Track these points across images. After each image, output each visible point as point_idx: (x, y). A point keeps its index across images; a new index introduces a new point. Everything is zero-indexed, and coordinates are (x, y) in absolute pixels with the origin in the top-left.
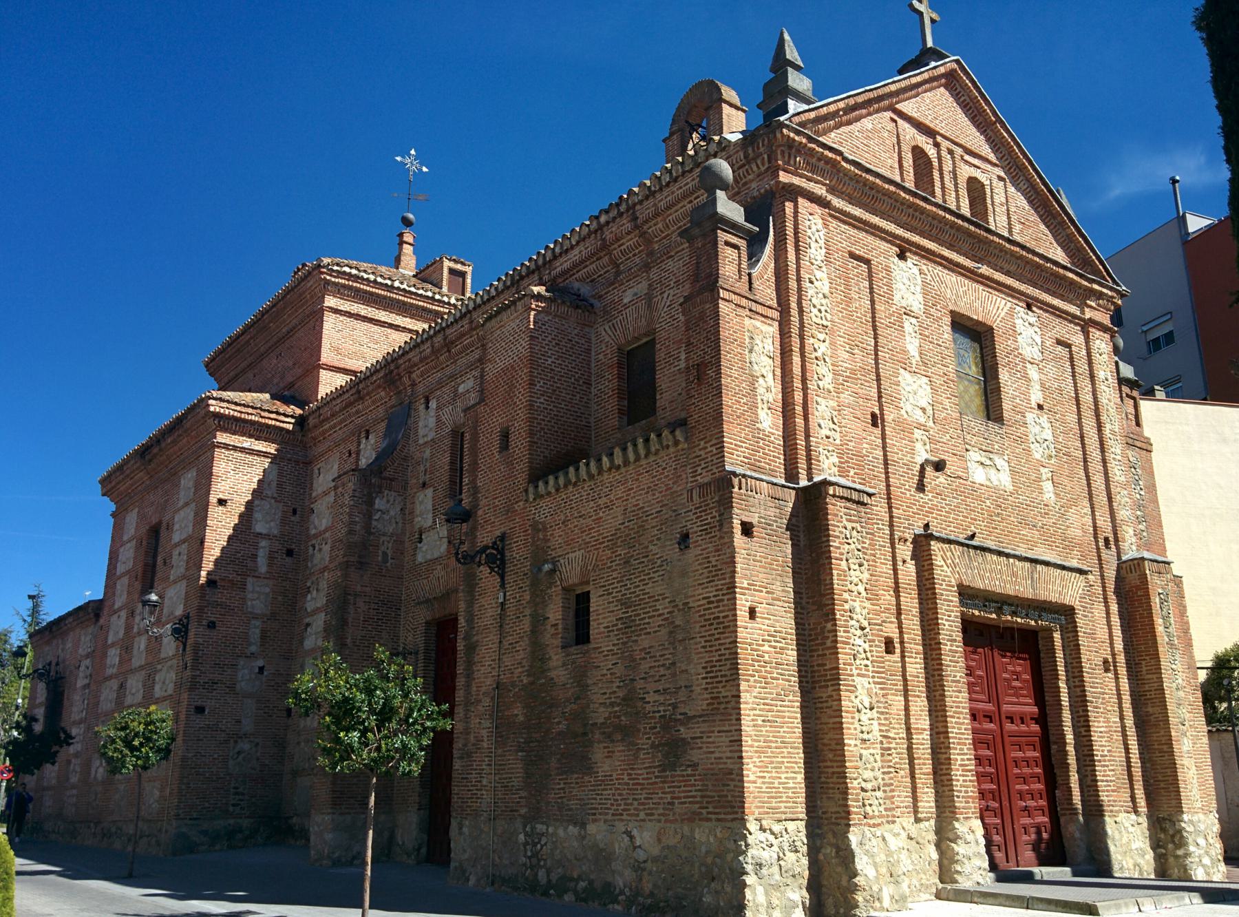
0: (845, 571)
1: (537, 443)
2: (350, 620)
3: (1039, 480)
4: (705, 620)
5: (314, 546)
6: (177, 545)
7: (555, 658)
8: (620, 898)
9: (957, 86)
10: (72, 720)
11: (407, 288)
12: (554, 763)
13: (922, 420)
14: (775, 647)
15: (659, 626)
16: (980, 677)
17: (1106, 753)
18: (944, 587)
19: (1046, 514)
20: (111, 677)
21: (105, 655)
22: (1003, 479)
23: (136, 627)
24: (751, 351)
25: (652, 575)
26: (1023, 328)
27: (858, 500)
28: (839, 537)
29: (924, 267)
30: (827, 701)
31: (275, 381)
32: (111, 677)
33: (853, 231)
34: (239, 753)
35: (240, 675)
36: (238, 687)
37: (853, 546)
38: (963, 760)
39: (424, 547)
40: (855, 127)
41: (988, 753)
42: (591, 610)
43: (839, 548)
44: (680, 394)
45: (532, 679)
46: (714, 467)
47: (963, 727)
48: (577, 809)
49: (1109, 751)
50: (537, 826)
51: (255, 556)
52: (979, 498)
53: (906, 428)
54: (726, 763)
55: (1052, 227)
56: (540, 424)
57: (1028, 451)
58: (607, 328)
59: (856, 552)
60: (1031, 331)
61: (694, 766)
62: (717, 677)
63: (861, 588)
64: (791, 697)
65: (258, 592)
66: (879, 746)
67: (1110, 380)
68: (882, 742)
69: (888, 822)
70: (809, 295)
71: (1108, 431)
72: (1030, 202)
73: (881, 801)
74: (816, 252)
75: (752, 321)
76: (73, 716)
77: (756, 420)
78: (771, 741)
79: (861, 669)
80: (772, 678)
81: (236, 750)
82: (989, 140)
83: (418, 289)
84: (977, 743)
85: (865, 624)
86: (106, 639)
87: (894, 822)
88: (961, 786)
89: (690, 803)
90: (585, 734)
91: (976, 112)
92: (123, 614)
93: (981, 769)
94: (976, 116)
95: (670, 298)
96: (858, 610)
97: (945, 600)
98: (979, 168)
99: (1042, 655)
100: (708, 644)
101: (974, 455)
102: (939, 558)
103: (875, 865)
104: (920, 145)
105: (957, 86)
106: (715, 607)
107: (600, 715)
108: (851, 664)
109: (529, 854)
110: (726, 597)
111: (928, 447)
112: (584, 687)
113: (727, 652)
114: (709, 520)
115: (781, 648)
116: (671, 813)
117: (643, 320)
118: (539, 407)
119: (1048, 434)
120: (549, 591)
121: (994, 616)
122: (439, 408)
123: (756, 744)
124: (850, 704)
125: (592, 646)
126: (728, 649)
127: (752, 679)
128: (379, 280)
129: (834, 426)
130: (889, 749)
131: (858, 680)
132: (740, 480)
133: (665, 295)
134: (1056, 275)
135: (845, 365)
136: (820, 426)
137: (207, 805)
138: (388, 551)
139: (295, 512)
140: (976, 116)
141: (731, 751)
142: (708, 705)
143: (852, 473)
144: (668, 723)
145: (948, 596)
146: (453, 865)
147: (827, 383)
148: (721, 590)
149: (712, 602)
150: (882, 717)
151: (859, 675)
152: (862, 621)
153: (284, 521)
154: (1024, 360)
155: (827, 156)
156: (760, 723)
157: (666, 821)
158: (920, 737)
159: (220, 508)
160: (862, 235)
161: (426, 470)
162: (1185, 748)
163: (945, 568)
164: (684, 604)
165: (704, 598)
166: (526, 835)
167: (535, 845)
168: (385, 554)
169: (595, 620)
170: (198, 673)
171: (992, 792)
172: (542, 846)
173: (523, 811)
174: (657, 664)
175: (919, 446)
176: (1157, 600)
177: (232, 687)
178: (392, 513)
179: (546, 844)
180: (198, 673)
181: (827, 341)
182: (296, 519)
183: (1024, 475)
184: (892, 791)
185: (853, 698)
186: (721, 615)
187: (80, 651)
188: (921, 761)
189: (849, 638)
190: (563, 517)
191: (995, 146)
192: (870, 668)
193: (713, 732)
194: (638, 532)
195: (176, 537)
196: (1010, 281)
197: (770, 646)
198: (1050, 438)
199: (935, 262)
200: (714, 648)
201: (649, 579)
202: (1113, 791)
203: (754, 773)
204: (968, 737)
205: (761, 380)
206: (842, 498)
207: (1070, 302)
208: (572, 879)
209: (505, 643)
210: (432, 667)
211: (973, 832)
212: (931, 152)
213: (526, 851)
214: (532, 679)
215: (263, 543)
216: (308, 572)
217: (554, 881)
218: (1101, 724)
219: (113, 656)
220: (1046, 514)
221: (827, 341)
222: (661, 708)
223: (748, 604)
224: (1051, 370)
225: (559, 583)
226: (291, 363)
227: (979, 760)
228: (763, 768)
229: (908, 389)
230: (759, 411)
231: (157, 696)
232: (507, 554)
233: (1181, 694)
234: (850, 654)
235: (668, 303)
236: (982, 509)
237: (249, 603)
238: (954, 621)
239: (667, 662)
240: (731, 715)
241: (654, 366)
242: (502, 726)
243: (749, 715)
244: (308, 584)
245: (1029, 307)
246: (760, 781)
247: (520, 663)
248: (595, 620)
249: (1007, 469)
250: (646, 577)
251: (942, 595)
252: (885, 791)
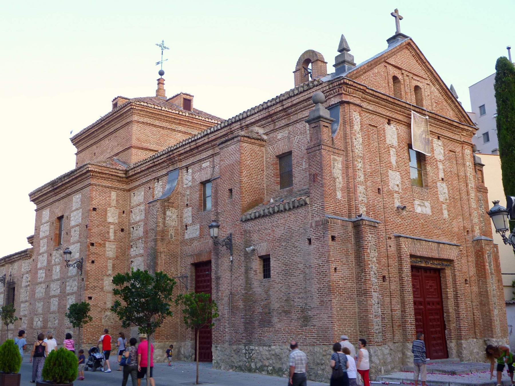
0: (369, 253)
1: (244, 197)
2: (159, 263)
3: (442, 210)
4: (318, 272)
5: (133, 228)
6: (73, 227)
7: (255, 284)
8: (285, 373)
10: (21, 300)
11: (168, 110)
12: (257, 323)
13: (397, 190)
14: (344, 282)
15: (299, 274)
16: (418, 289)
17: (465, 316)
18: (405, 256)
19: (444, 223)
20: (40, 283)
21: (37, 273)
22: (428, 211)
23: (53, 261)
24: (334, 168)
25: (296, 254)
26: (436, 147)
27: (374, 226)
28: (367, 240)
29: (398, 127)
30: (362, 302)
31: (108, 151)
32: (40, 283)
33: (371, 116)
34: (106, 316)
35: (105, 283)
36: (104, 288)
37: (372, 243)
38: (411, 321)
39: (188, 231)
41: (420, 317)
42: (271, 266)
43: (367, 245)
44: (303, 179)
45: (246, 291)
46: (321, 215)
47: (411, 308)
48: (267, 341)
49: (466, 315)
50: (250, 347)
51: (108, 232)
52: (418, 219)
53: (391, 193)
54: (326, 325)
56: (245, 189)
57: (438, 198)
58: (270, 148)
59: (373, 246)
60: (440, 148)
61: (314, 326)
62: (323, 293)
63: (374, 259)
64: (349, 300)
65: (110, 248)
66: (381, 317)
67: (471, 166)
68: (382, 316)
69: (384, 344)
70: (355, 144)
71: (470, 187)
74: (357, 127)
75: (334, 156)
76: (21, 298)
77: (336, 196)
78: (342, 316)
79: (374, 289)
80: (343, 293)
81: (105, 315)
83: (172, 110)
84: (416, 314)
85: (376, 272)
86: (37, 265)
87: (386, 344)
88: (410, 330)
89: (313, 338)
90: (269, 313)
92: (46, 255)
93: (417, 323)
95: (298, 139)
96: (374, 267)
97: (405, 261)
98: (419, 81)
99: (441, 279)
100: (319, 281)
101: (417, 202)
102: (403, 245)
103: (379, 359)
104: (396, 75)
106: (322, 268)
107: (275, 305)
108: (371, 288)
109: (247, 357)
110: (326, 264)
111: (399, 200)
112: (269, 296)
113: (327, 284)
114: (319, 235)
115: (346, 282)
116: (305, 342)
117: (286, 146)
118: (245, 182)
119: (446, 190)
120: (252, 257)
122: (193, 173)
123: (337, 317)
125: (272, 279)
126: (327, 283)
127: (336, 294)
128: (156, 107)
129: (364, 196)
130: (384, 318)
131: (373, 293)
132: (331, 220)
133: (296, 138)
135: (368, 171)
137: (94, 338)
138: (173, 234)
139: (124, 212)
141: (328, 320)
142: (319, 303)
143: (371, 214)
144: (303, 310)
145: (406, 259)
146: (213, 361)
147: (362, 178)
148: (324, 261)
149: (321, 266)
150: (382, 306)
151: (374, 291)
152: (375, 271)
153: (119, 217)
154: (437, 161)
156: (339, 310)
157: (303, 345)
158: (395, 312)
159: (94, 212)
160: (374, 116)
161: (188, 199)
162: (495, 313)
163: (405, 249)
164: (309, 266)
165: (317, 264)
166: (246, 350)
167: (250, 353)
168: (171, 235)
169: (273, 270)
170: (88, 283)
171: (420, 319)
172: (253, 354)
173: (244, 341)
174: (299, 288)
175: (396, 200)
176: (487, 256)
177: (102, 289)
178: (173, 217)
179: (254, 353)
180: (88, 283)
181: (362, 162)
182: (124, 215)
183: (436, 208)
184: (385, 333)
186: (324, 271)
187: (23, 270)
188: (395, 322)
189: (370, 278)
190: (258, 229)
192: (378, 289)
193: (321, 313)
194: (290, 237)
195: (73, 223)
197: (342, 282)
198: (447, 192)
200: (321, 283)
201: (295, 255)
202: (467, 330)
203: (337, 328)
204: (413, 312)
205: (337, 180)
208: (265, 366)
209: (233, 277)
210: (194, 282)
212: (400, 77)
213: (246, 356)
214: (246, 291)
215: (112, 226)
216: (131, 239)
217: (258, 367)
218: (463, 305)
219: (41, 274)
220: (444, 223)
221: (362, 162)
222: (301, 304)
223: (334, 267)
224: (447, 164)
225: (257, 255)
226: (116, 144)
227: (417, 320)
228: (340, 326)
229: (392, 177)
230: (337, 192)
231: (67, 292)
232: (233, 241)
233: (495, 292)
235: (297, 141)
236: (420, 223)
237: (107, 253)
238: (408, 269)
239: (303, 287)
240: (328, 307)
241: (292, 167)
242: (233, 309)
243: (334, 307)
244: (131, 244)
245: (439, 138)
246: (338, 330)
247: (241, 285)
248: (273, 270)
249: (429, 206)
250: (294, 255)
251: (404, 259)
252: (383, 333)
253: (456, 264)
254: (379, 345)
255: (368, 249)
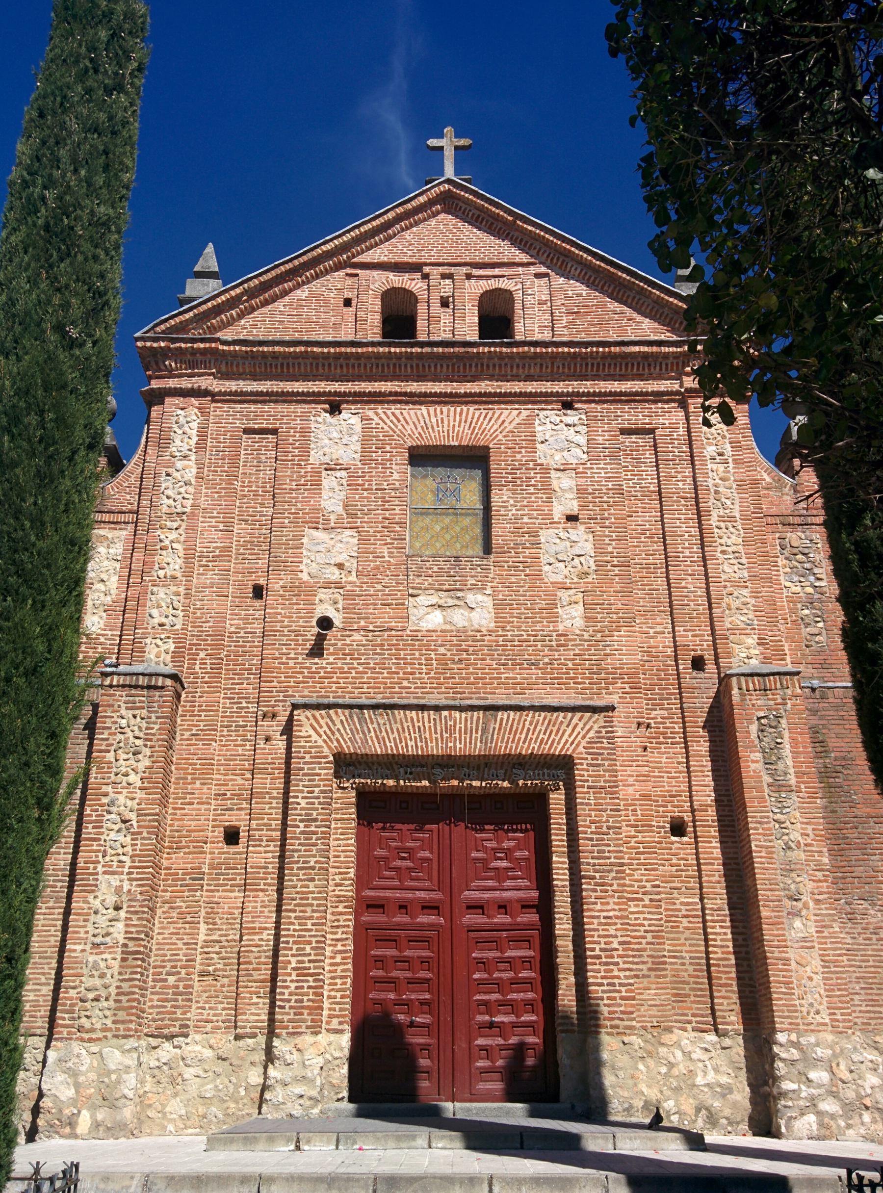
9: (461, 204)
40: (279, 305)
55: (629, 301)
68: (125, 945)
72: (590, 284)
73: (107, 1013)
82: (515, 242)
91: (491, 220)
94: (492, 224)
98: (503, 276)
105: (461, 204)
121: (426, 783)
124: (85, 906)
134: (615, 356)
136: (150, 616)
140: (492, 224)
151: (105, 873)
154: (545, 470)
155: (199, 349)
176: (754, 728)
185: (91, 898)
191: (525, 245)
196: (516, 387)
199: (388, 402)
206: (123, 686)
207: (660, 378)
211: (299, 1050)
234: (99, 851)
253: (583, 773)
254: (90, 1040)
255: (109, 751)
